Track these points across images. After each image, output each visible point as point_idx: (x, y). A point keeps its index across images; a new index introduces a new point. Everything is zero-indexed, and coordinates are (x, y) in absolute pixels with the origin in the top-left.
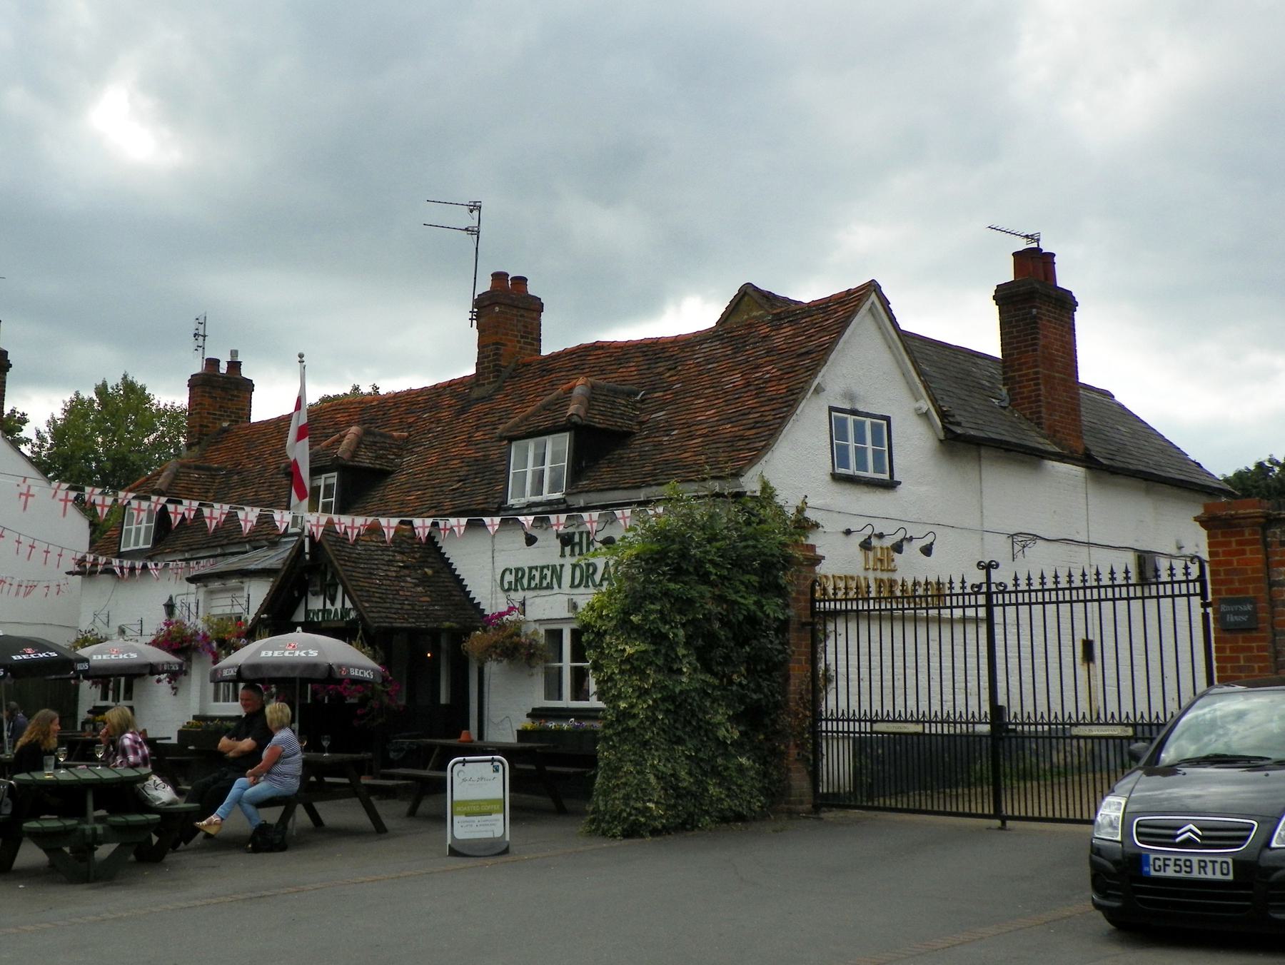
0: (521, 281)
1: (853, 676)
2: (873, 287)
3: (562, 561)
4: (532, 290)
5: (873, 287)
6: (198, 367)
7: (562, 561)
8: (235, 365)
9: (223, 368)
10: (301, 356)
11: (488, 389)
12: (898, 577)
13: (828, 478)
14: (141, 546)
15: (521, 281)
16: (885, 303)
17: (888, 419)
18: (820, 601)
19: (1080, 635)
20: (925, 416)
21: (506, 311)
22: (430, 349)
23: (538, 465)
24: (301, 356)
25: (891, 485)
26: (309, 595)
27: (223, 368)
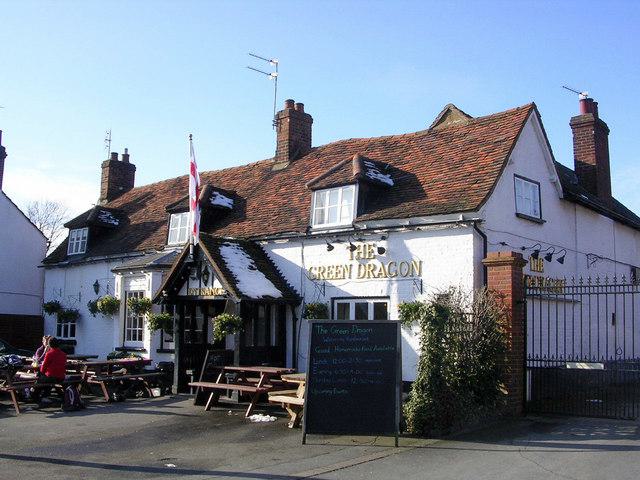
0: (301, 106)
1: (537, 337)
2: (533, 106)
3: (351, 262)
4: (306, 111)
5: (533, 106)
6: (107, 157)
7: (351, 262)
8: (126, 156)
9: (120, 158)
10: (191, 136)
11: (285, 165)
12: (544, 275)
13: (514, 216)
14: (79, 252)
15: (301, 106)
16: (539, 116)
17: (539, 184)
18: (530, 289)
19: (611, 311)
20: (555, 183)
21: (296, 123)
22: (255, 144)
23: (339, 207)
24: (191, 136)
25: (540, 222)
26: (191, 281)
27: (120, 158)
